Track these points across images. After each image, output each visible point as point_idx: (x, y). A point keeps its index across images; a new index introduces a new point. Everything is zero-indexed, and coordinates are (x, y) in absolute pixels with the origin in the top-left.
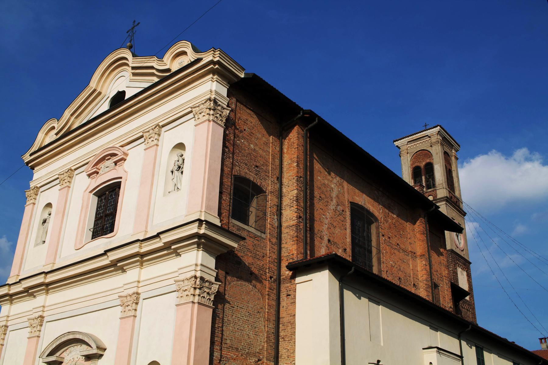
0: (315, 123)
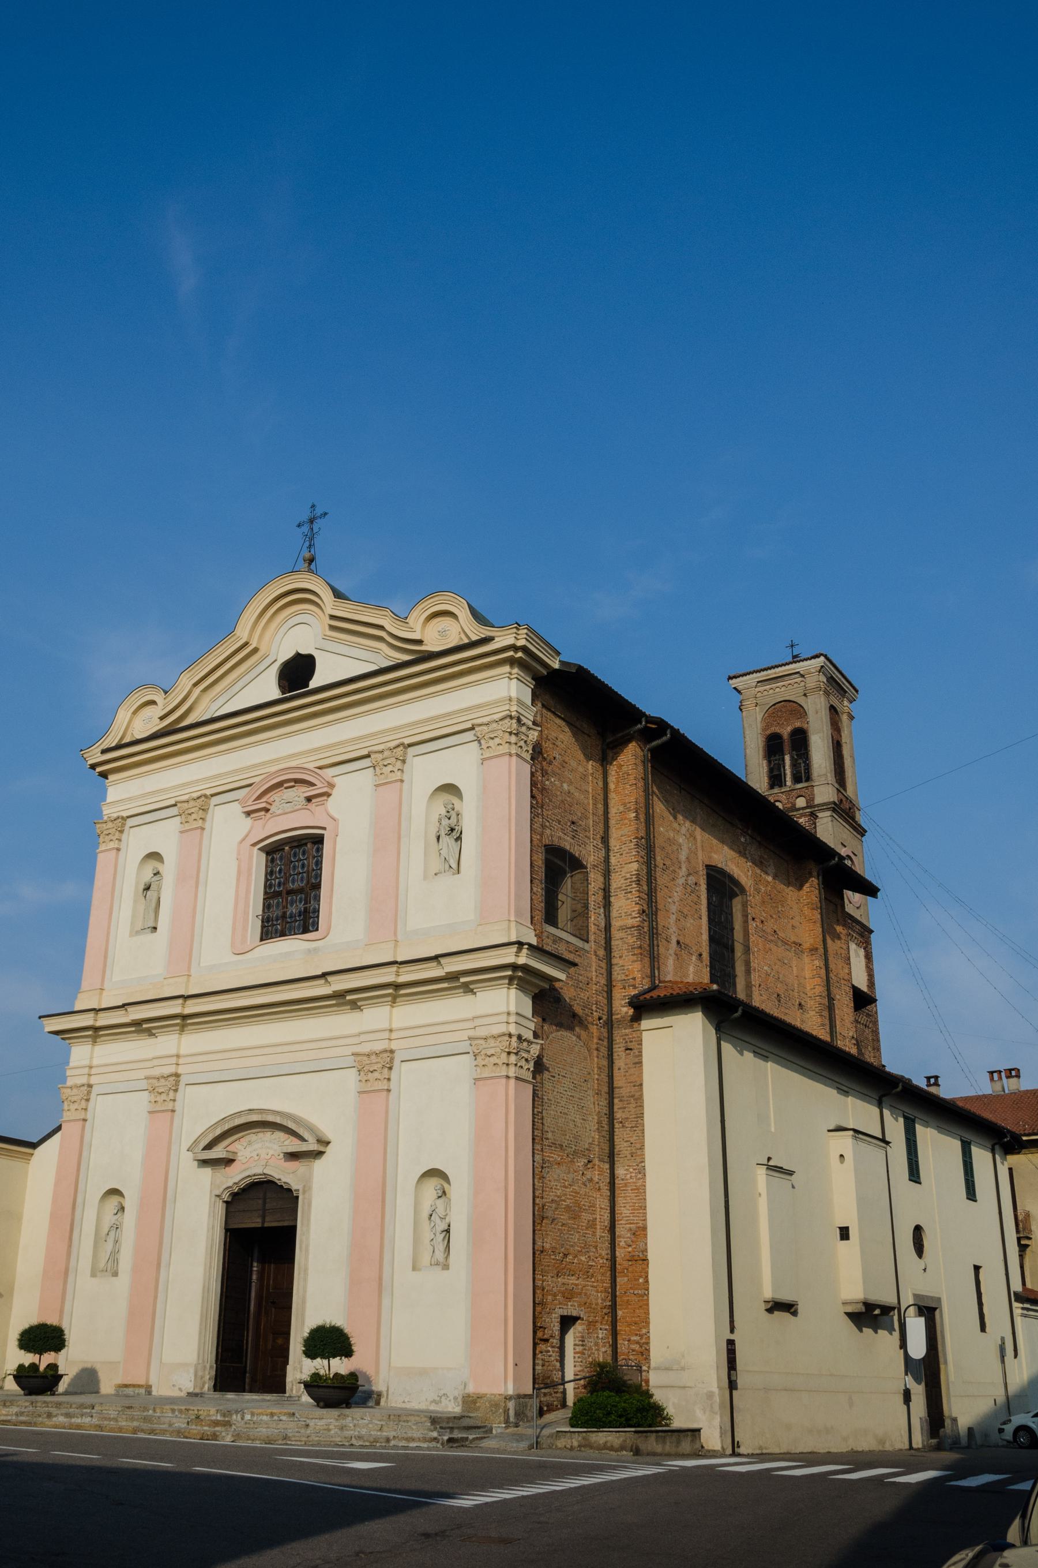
0: (664, 739)
